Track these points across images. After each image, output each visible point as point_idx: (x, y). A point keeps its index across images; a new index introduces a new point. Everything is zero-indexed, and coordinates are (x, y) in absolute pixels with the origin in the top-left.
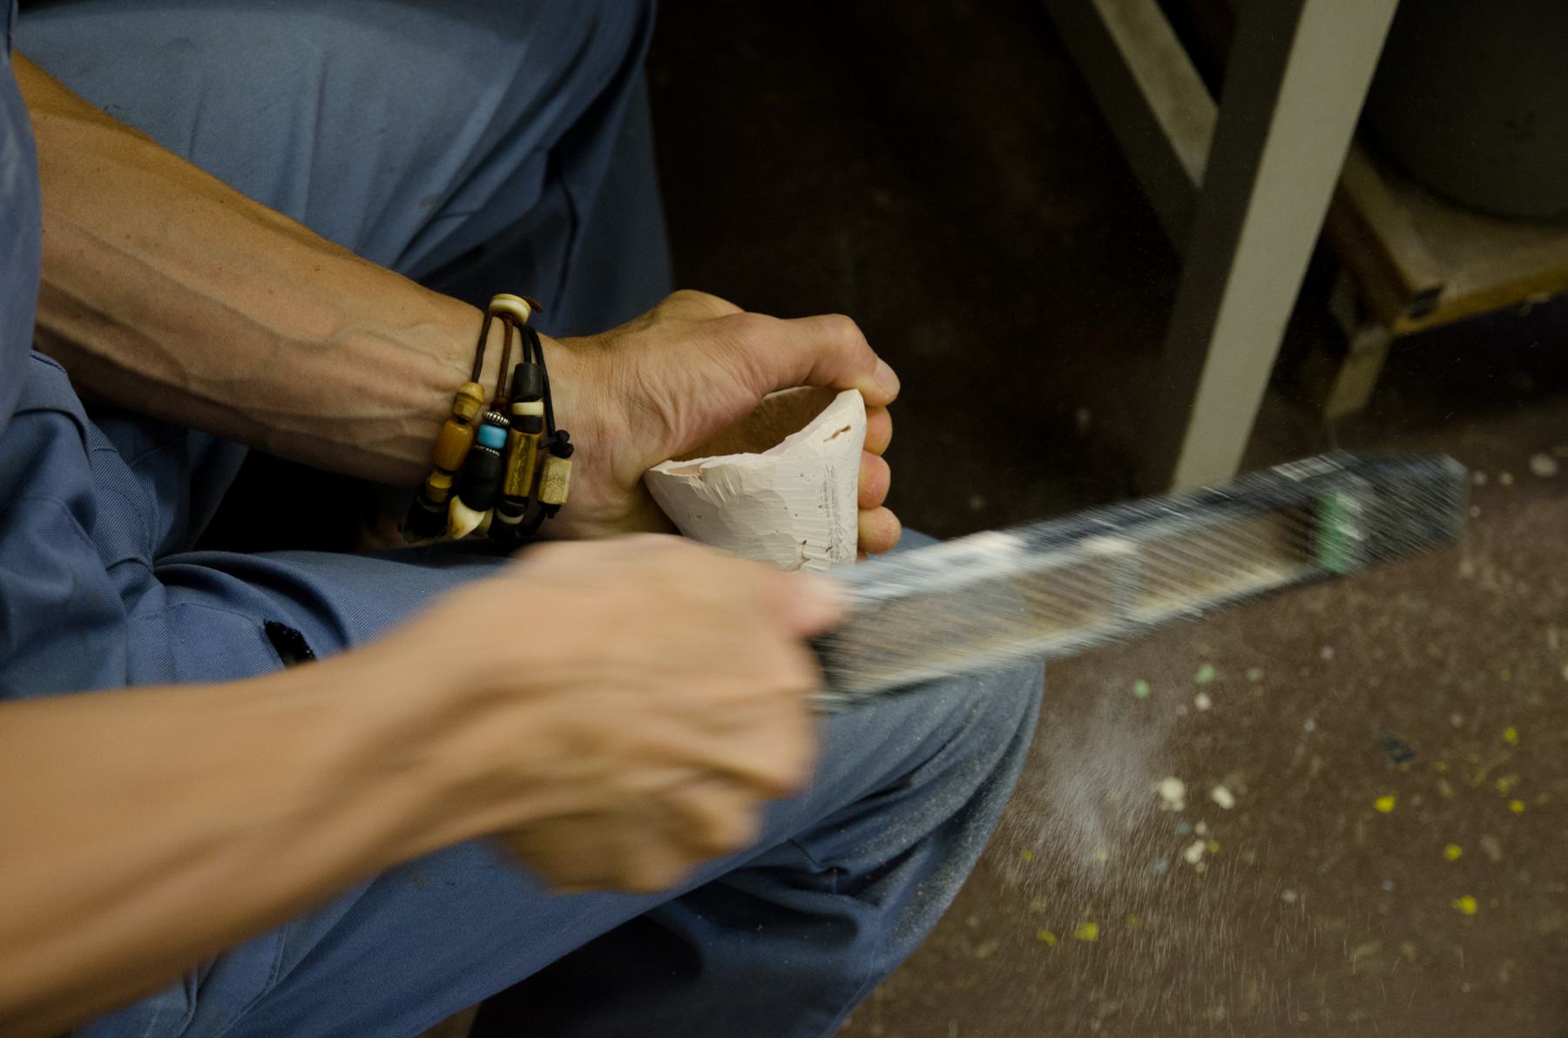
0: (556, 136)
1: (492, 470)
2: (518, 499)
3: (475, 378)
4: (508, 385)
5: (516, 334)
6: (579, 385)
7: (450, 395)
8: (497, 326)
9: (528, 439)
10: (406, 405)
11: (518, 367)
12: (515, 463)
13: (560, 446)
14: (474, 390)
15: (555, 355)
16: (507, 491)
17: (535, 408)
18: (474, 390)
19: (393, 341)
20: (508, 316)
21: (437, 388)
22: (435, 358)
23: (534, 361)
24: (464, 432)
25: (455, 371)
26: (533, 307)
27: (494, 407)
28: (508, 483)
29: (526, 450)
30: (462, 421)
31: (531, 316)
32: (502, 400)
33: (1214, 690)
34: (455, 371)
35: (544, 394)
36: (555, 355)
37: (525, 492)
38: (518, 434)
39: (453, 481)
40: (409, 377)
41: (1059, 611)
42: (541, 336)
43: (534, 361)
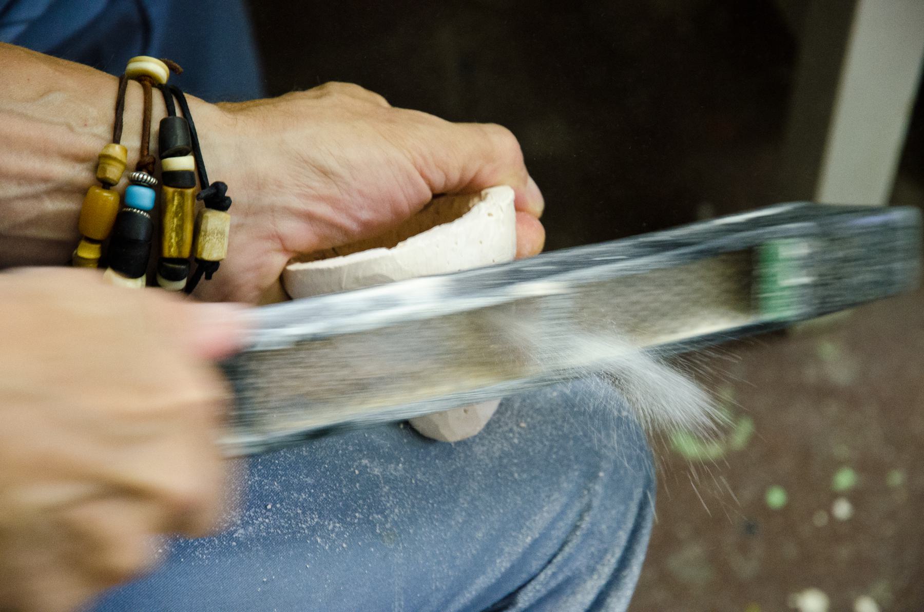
0: (244, 105)
1: (142, 233)
2: (179, 261)
3: (116, 139)
4: (153, 145)
5: (157, 98)
6: (232, 139)
7: (90, 165)
8: (134, 92)
9: (182, 195)
10: (45, 180)
11: (163, 123)
12: (171, 222)
13: (217, 198)
14: (116, 150)
15: (203, 113)
16: (166, 254)
17: (185, 163)
18: (116, 150)
19: (22, 115)
20: (146, 79)
21: (78, 159)
22: (71, 129)
23: (178, 113)
24: (109, 198)
25: (93, 138)
26: (172, 69)
27: (140, 167)
28: (166, 245)
29: (181, 206)
30: (106, 184)
31: (170, 78)
32: (147, 159)
33: (854, 496)
34: (93, 138)
35: (193, 148)
36: (203, 113)
37: (186, 253)
38: (170, 190)
39: (103, 251)
40: (44, 151)
41: (699, 438)
42: (186, 95)
43: (178, 113)
